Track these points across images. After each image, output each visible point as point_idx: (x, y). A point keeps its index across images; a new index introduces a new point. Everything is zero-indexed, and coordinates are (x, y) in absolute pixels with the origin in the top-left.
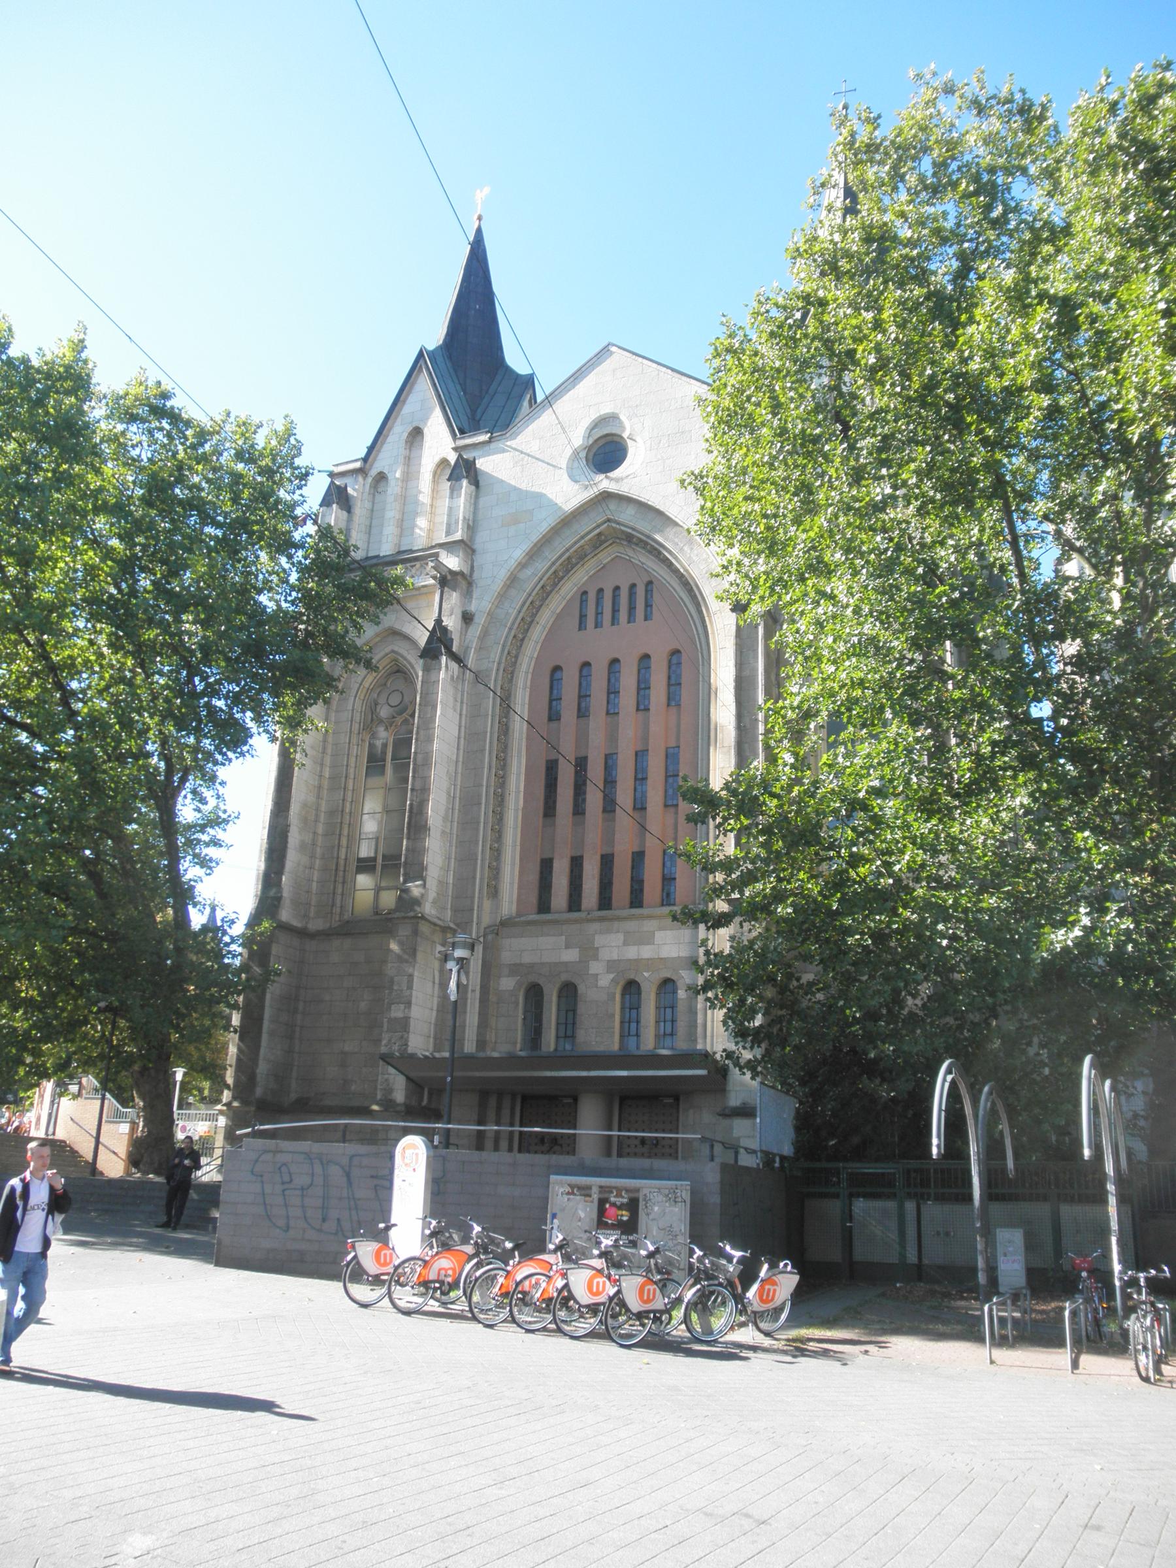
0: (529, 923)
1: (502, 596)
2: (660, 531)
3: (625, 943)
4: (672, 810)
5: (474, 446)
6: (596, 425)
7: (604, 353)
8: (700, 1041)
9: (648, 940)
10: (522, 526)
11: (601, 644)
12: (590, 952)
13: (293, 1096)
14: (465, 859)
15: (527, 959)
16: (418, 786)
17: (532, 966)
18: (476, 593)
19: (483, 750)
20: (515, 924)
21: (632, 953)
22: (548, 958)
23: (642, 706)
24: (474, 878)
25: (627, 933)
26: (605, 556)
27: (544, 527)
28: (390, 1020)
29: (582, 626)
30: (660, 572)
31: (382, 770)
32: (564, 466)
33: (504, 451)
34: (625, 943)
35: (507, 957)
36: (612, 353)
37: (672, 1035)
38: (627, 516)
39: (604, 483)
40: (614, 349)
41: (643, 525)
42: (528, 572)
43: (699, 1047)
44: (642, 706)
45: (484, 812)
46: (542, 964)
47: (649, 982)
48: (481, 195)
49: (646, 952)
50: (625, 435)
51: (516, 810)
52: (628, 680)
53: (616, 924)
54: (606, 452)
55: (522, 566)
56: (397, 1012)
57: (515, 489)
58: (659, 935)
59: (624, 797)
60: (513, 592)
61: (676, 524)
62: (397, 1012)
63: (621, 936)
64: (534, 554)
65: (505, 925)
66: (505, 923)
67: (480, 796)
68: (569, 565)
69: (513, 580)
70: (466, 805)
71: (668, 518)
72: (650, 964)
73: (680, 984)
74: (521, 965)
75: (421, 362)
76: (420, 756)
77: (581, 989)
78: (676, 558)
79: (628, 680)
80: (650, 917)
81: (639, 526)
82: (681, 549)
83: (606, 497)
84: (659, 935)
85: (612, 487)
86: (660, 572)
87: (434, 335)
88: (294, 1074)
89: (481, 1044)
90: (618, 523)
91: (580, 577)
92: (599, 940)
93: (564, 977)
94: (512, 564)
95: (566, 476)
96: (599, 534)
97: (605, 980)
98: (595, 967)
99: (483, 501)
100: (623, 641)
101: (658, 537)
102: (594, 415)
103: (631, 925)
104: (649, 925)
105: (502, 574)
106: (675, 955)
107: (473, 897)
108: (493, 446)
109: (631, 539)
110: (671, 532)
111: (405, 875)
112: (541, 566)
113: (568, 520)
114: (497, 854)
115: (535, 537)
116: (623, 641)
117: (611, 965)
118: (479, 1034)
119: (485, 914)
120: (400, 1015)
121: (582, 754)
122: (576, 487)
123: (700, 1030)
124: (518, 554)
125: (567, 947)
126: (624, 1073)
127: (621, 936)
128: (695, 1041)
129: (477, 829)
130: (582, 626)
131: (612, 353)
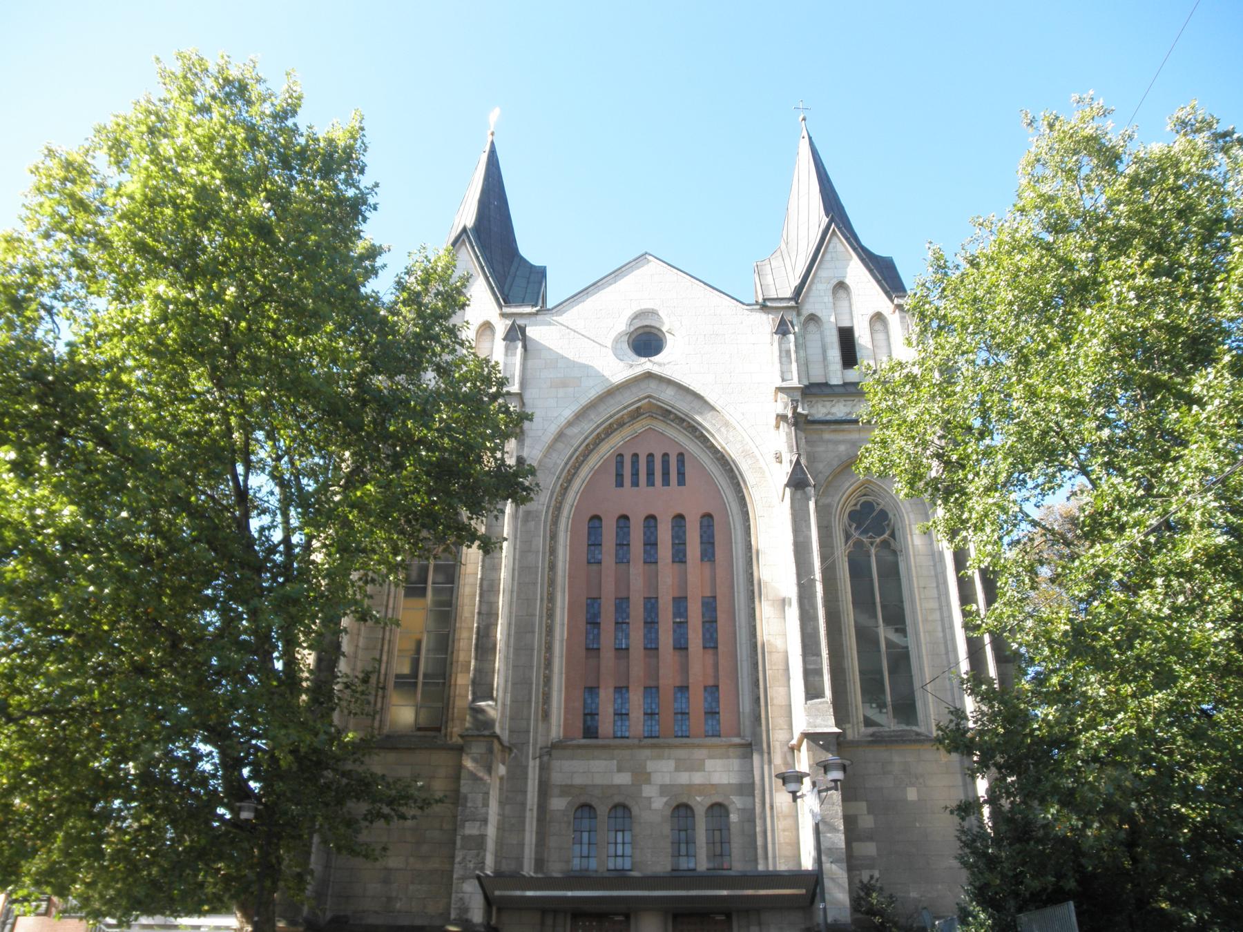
0: (580, 747)
1: (551, 447)
2: (701, 413)
3: (677, 769)
4: (711, 651)
5: (522, 315)
6: (637, 316)
7: (641, 259)
8: (761, 861)
9: (700, 767)
10: (571, 390)
11: (638, 501)
12: (642, 776)
13: (329, 915)
14: (520, 682)
15: (578, 780)
16: (484, 610)
17: (583, 788)
18: (528, 442)
19: (535, 584)
20: (565, 748)
21: (684, 778)
22: (599, 780)
23: (679, 556)
24: (530, 701)
25: (678, 760)
26: (639, 426)
27: (593, 394)
28: (464, 837)
29: (620, 483)
30: (692, 447)
31: (422, 593)
32: (609, 345)
33: (550, 324)
34: (677, 769)
35: (557, 778)
36: (649, 261)
37: (721, 855)
38: (667, 396)
39: (646, 365)
40: (650, 258)
41: (682, 405)
42: (575, 430)
43: (761, 867)
44: (679, 556)
45: (537, 640)
46: (594, 786)
47: (700, 803)
48: (494, 116)
49: (698, 778)
50: (664, 329)
51: (562, 641)
52: (665, 534)
53: (616, 752)
54: (646, 341)
55: (570, 424)
56: (471, 829)
57: (563, 357)
58: (709, 764)
59: (666, 638)
60: (560, 446)
61: (713, 408)
62: (471, 829)
63: (671, 764)
64: (581, 415)
65: (553, 749)
66: (554, 746)
67: (533, 625)
68: (609, 431)
69: (560, 436)
70: (521, 630)
71: (706, 402)
72: (702, 789)
73: (731, 808)
74: (572, 786)
75: (464, 236)
76: (485, 583)
77: (635, 810)
78: (713, 436)
79: (665, 534)
80: (699, 746)
81: (677, 405)
82: (719, 430)
83: (649, 376)
84: (709, 764)
85: (656, 370)
86: (692, 447)
87: (468, 216)
88: (330, 892)
89: (540, 863)
90: (658, 400)
91: (616, 441)
92: (651, 766)
93: (617, 799)
94: (562, 421)
95: (611, 353)
96: (638, 408)
97: (659, 803)
98: (648, 791)
99: (530, 363)
100: (663, 501)
101: (698, 418)
102: (636, 308)
103: (682, 753)
104: (699, 754)
105: (553, 429)
106: (726, 782)
107: (529, 719)
108: (539, 317)
109: (666, 414)
110: (709, 415)
111: (474, 693)
112: (588, 427)
113: (613, 392)
114: (548, 680)
115: (584, 401)
116: (663, 501)
117: (664, 790)
118: (537, 853)
119: (537, 738)
120: (475, 832)
121: (624, 595)
122: (622, 364)
123: (760, 851)
124: (568, 413)
125: (620, 770)
126: (725, 893)
127: (672, 764)
128: (756, 861)
129: (532, 656)
130: (620, 483)
131: (649, 261)
